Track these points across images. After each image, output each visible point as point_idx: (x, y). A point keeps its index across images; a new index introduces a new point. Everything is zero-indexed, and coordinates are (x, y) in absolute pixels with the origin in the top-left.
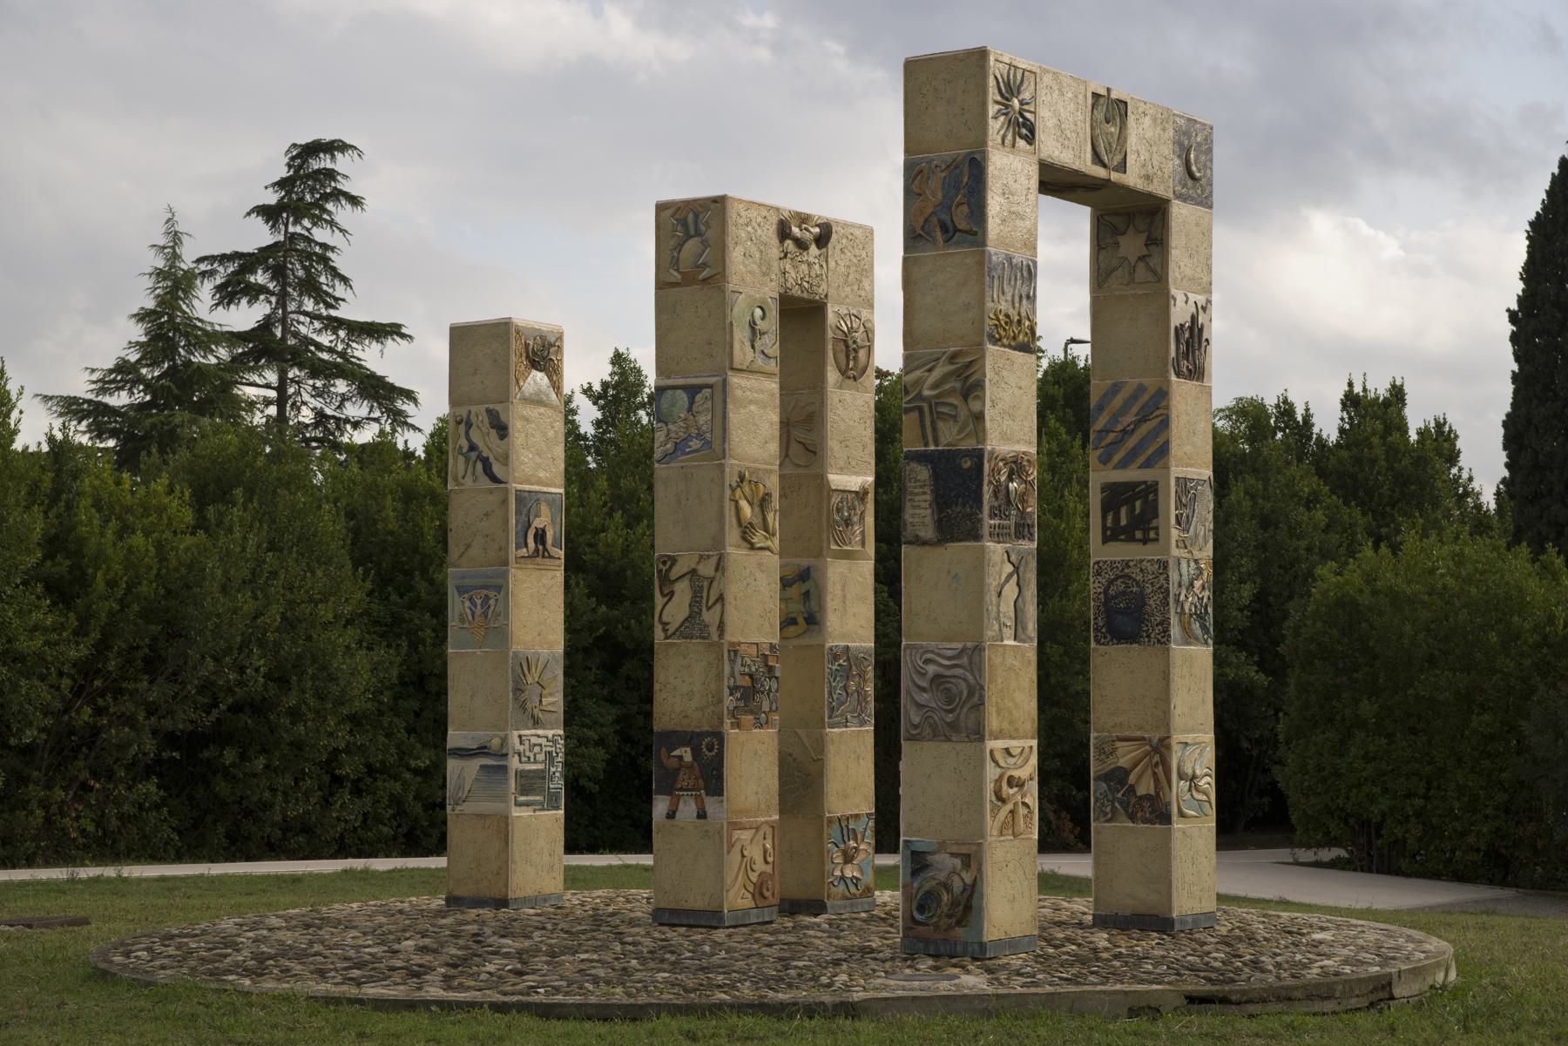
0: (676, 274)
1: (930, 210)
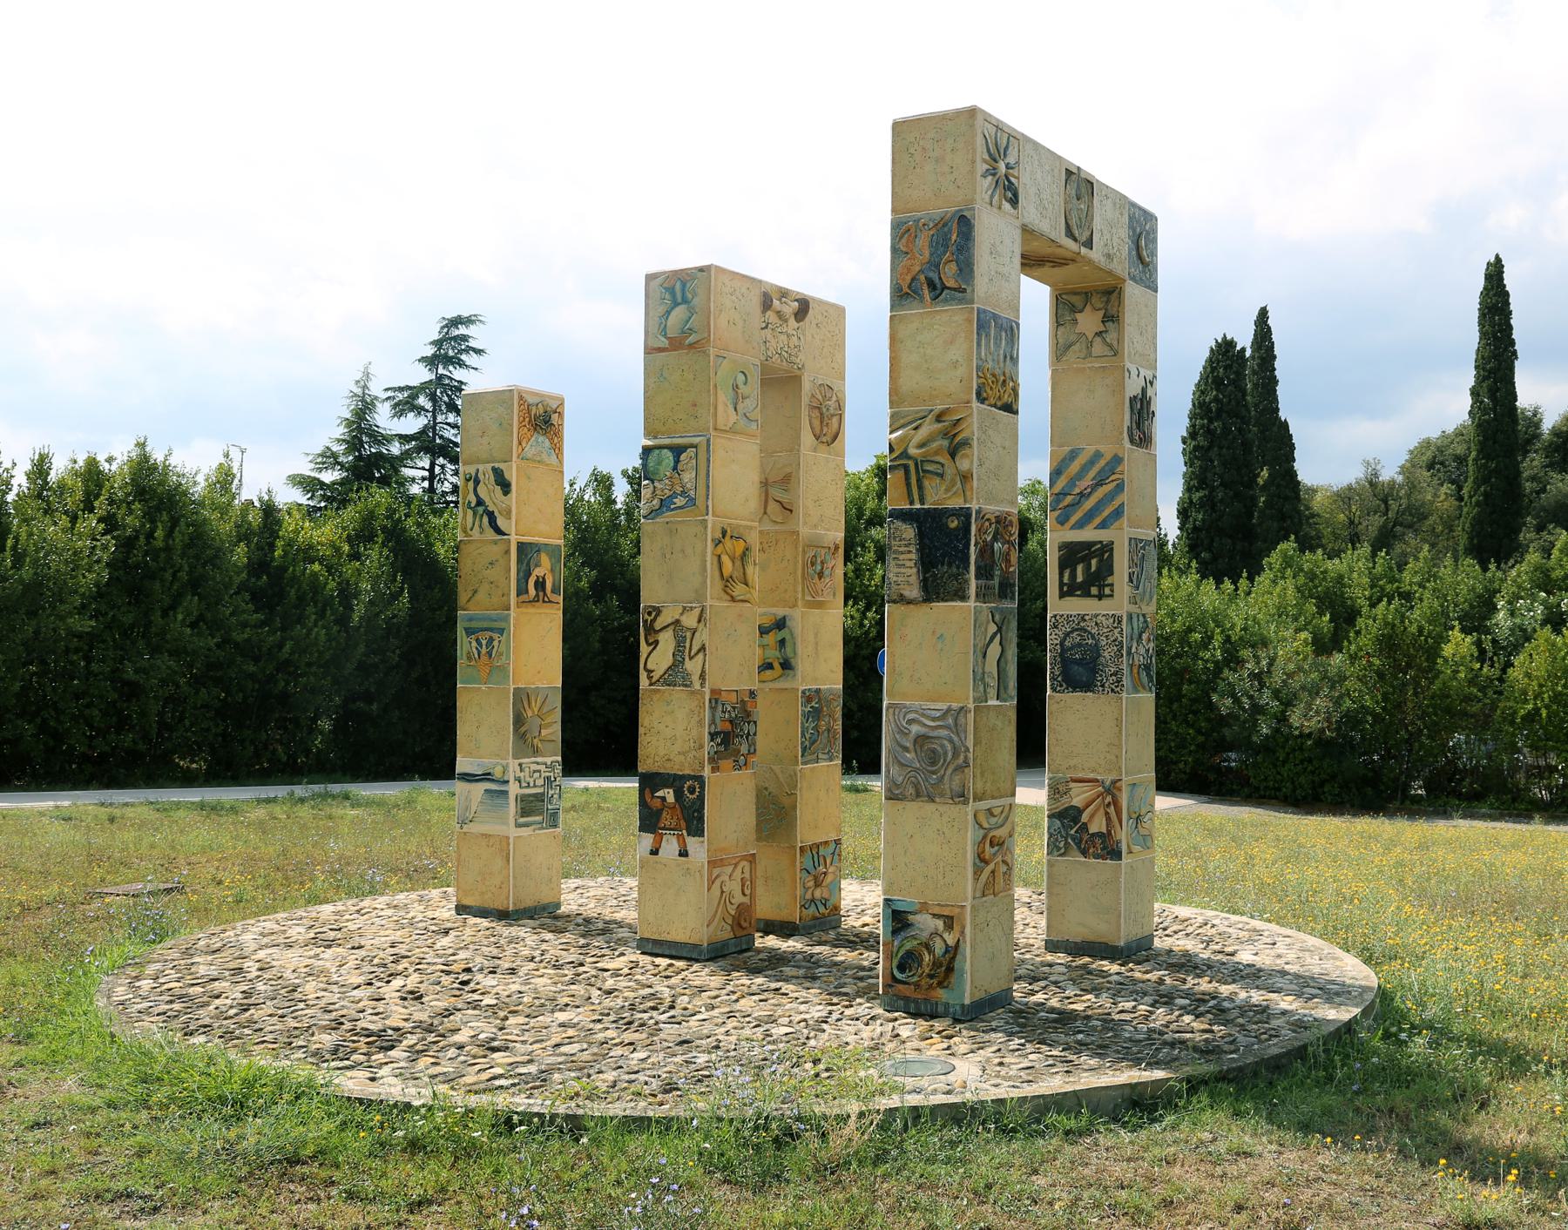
0: (663, 339)
1: (918, 268)
